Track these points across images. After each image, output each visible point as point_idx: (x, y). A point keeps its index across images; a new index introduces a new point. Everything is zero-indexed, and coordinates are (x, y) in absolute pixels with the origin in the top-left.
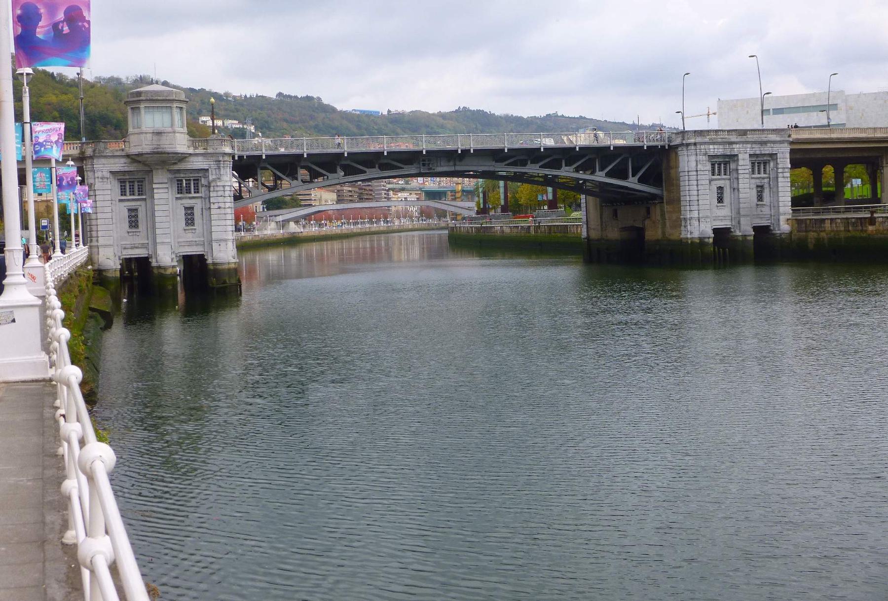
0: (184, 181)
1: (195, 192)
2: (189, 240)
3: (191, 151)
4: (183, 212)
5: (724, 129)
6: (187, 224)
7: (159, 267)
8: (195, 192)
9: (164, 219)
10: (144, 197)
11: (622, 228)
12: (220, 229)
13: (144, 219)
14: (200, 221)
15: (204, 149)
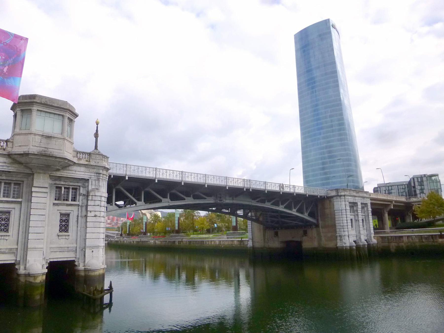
0: (63, 188)
1: (72, 200)
3: (75, 160)
4: (58, 218)
5: (396, 185)
6: (61, 230)
7: (29, 275)
8: (72, 200)
9: (39, 224)
11: (281, 242)
12: (94, 236)
13: (17, 224)
14: (75, 228)
15: (87, 161)
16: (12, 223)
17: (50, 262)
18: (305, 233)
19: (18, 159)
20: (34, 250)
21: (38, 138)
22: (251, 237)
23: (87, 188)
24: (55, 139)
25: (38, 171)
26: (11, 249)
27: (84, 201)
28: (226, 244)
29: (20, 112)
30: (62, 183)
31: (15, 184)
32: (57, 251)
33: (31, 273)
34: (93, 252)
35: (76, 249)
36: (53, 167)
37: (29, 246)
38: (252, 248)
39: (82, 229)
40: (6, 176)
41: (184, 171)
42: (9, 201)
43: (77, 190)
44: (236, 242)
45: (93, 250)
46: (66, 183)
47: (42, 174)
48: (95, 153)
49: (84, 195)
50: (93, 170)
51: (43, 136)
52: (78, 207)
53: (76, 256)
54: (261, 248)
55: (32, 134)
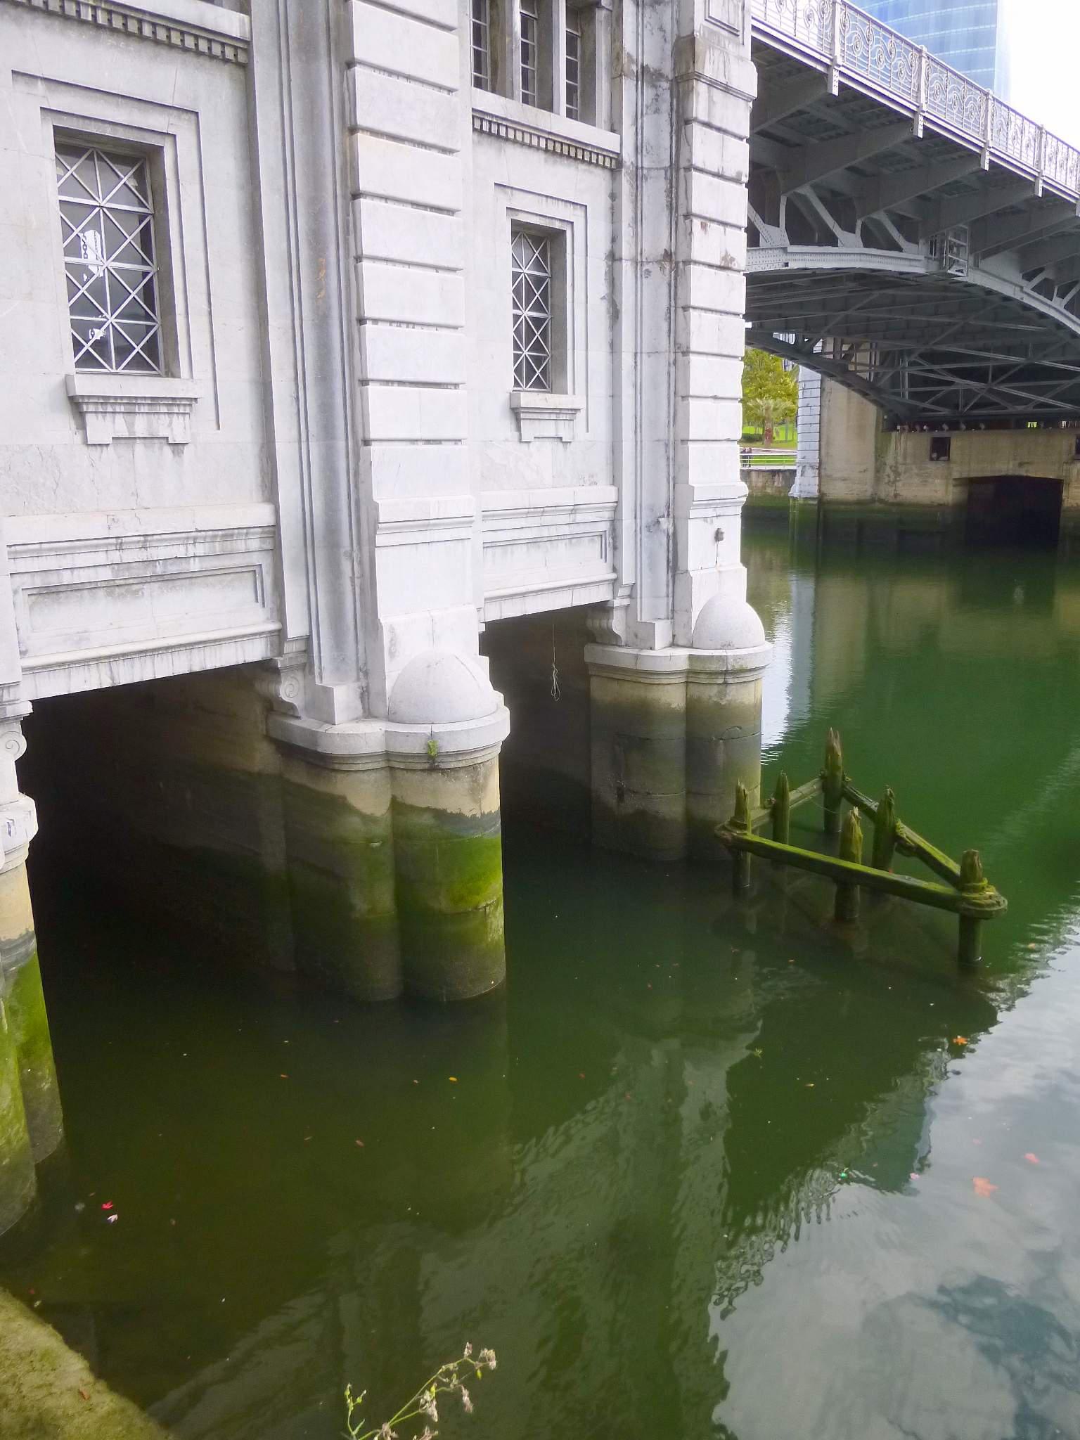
14: (599, 355)
20: (419, 537)
26: (228, 534)
32: (513, 543)
35: (615, 523)
38: (816, 502)
43: (592, 19)
45: (718, 524)
52: (607, 174)
54: (859, 503)
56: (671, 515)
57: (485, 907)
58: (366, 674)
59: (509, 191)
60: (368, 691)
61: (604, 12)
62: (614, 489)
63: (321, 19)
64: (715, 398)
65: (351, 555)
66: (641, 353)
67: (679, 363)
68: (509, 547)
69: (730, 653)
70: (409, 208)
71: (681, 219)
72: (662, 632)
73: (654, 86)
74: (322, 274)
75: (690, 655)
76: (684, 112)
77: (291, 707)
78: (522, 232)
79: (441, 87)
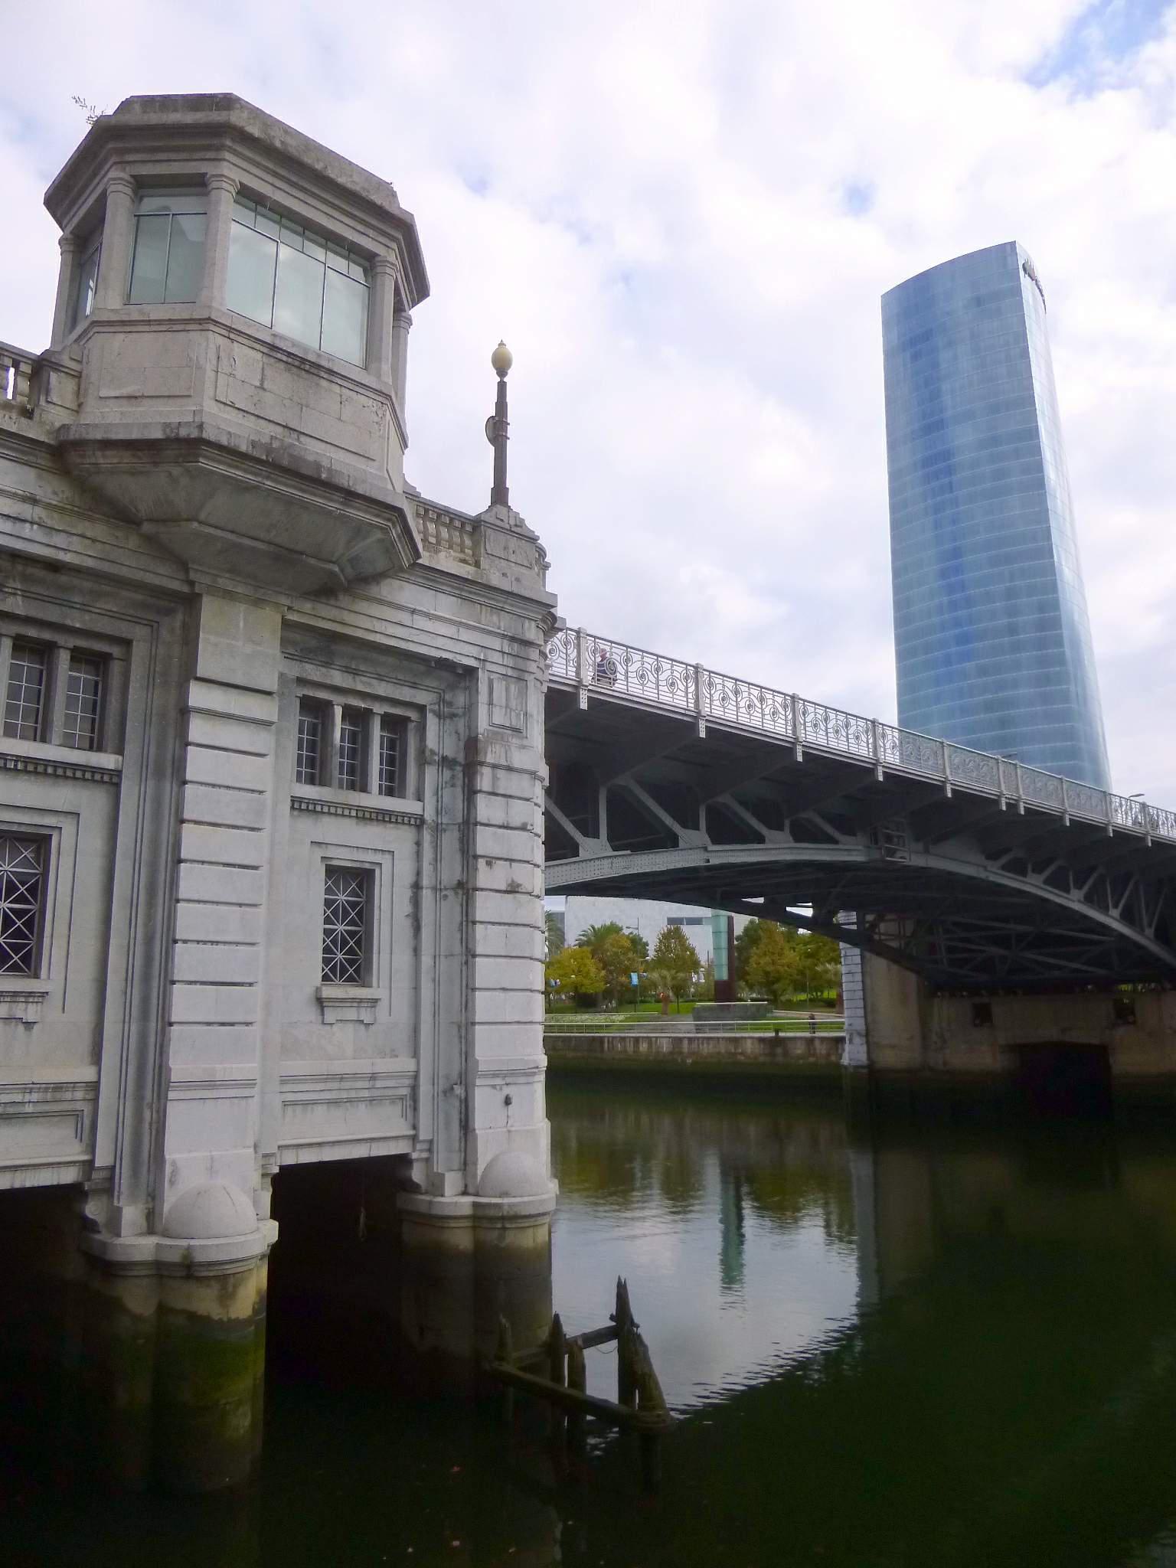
2: (338, 1067)
6: (332, 972)
9: (231, 921)
10: (107, 760)
14: (403, 959)
16: (62, 912)
17: (282, 1168)
18: (1124, 1014)
19: (113, 486)
21: (246, 359)
22: (860, 1024)
23: (461, 724)
24: (337, 389)
25: (224, 582)
26: (58, 1087)
27: (447, 793)
28: (706, 1051)
29: (129, 191)
30: (338, 678)
31: (78, 657)
32: (315, 1102)
33: (200, 1257)
34: (508, 1101)
35: (415, 1088)
36: (312, 561)
37: (180, 1066)
39: (443, 964)
40: (26, 595)
41: (800, 697)
42: (46, 763)
44: (753, 1044)
45: (507, 1091)
46: (358, 678)
47: (242, 607)
48: (499, 523)
49: (446, 762)
50: (495, 618)
51: (274, 354)
52: (413, 830)
53: (415, 1127)
55: (212, 327)
56: (463, 1082)
57: (225, 1404)
58: (153, 1198)
59: (324, 846)
60: (153, 1212)
61: (414, 724)
62: (413, 1061)
63: (169, 756)
64: (504, 989)
65: (152, 1106)
66: (439, 955)
67: (470, 963)
68: (310, 1106)
69: (506, 1200)
70: (221, 868)
71: (471, 858)
72: (452, 1183)
73: (451, 769)
74: (152, 911)
75: (474, 1202)
76: (473, 786)
77: (94, 1223)
78: (335, 873)
79: (253, 791)
